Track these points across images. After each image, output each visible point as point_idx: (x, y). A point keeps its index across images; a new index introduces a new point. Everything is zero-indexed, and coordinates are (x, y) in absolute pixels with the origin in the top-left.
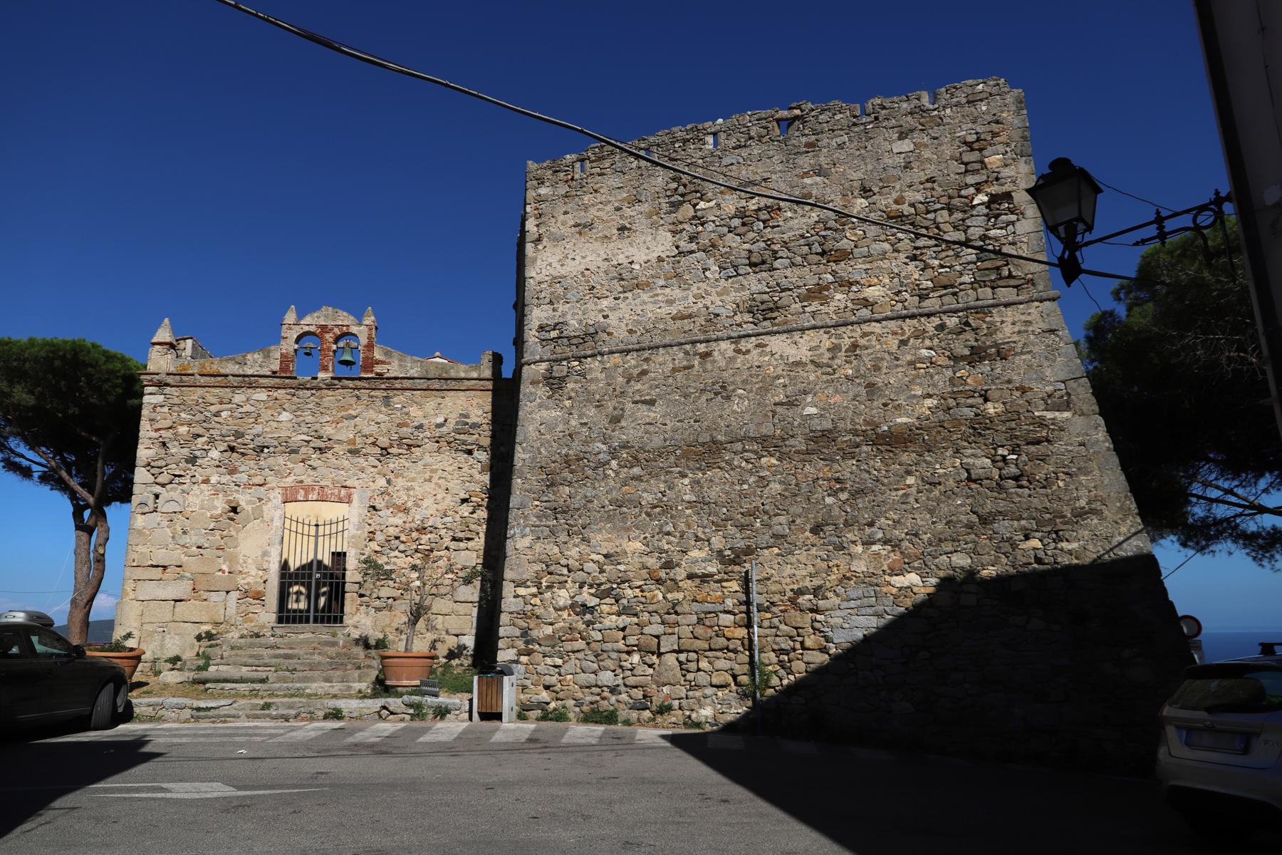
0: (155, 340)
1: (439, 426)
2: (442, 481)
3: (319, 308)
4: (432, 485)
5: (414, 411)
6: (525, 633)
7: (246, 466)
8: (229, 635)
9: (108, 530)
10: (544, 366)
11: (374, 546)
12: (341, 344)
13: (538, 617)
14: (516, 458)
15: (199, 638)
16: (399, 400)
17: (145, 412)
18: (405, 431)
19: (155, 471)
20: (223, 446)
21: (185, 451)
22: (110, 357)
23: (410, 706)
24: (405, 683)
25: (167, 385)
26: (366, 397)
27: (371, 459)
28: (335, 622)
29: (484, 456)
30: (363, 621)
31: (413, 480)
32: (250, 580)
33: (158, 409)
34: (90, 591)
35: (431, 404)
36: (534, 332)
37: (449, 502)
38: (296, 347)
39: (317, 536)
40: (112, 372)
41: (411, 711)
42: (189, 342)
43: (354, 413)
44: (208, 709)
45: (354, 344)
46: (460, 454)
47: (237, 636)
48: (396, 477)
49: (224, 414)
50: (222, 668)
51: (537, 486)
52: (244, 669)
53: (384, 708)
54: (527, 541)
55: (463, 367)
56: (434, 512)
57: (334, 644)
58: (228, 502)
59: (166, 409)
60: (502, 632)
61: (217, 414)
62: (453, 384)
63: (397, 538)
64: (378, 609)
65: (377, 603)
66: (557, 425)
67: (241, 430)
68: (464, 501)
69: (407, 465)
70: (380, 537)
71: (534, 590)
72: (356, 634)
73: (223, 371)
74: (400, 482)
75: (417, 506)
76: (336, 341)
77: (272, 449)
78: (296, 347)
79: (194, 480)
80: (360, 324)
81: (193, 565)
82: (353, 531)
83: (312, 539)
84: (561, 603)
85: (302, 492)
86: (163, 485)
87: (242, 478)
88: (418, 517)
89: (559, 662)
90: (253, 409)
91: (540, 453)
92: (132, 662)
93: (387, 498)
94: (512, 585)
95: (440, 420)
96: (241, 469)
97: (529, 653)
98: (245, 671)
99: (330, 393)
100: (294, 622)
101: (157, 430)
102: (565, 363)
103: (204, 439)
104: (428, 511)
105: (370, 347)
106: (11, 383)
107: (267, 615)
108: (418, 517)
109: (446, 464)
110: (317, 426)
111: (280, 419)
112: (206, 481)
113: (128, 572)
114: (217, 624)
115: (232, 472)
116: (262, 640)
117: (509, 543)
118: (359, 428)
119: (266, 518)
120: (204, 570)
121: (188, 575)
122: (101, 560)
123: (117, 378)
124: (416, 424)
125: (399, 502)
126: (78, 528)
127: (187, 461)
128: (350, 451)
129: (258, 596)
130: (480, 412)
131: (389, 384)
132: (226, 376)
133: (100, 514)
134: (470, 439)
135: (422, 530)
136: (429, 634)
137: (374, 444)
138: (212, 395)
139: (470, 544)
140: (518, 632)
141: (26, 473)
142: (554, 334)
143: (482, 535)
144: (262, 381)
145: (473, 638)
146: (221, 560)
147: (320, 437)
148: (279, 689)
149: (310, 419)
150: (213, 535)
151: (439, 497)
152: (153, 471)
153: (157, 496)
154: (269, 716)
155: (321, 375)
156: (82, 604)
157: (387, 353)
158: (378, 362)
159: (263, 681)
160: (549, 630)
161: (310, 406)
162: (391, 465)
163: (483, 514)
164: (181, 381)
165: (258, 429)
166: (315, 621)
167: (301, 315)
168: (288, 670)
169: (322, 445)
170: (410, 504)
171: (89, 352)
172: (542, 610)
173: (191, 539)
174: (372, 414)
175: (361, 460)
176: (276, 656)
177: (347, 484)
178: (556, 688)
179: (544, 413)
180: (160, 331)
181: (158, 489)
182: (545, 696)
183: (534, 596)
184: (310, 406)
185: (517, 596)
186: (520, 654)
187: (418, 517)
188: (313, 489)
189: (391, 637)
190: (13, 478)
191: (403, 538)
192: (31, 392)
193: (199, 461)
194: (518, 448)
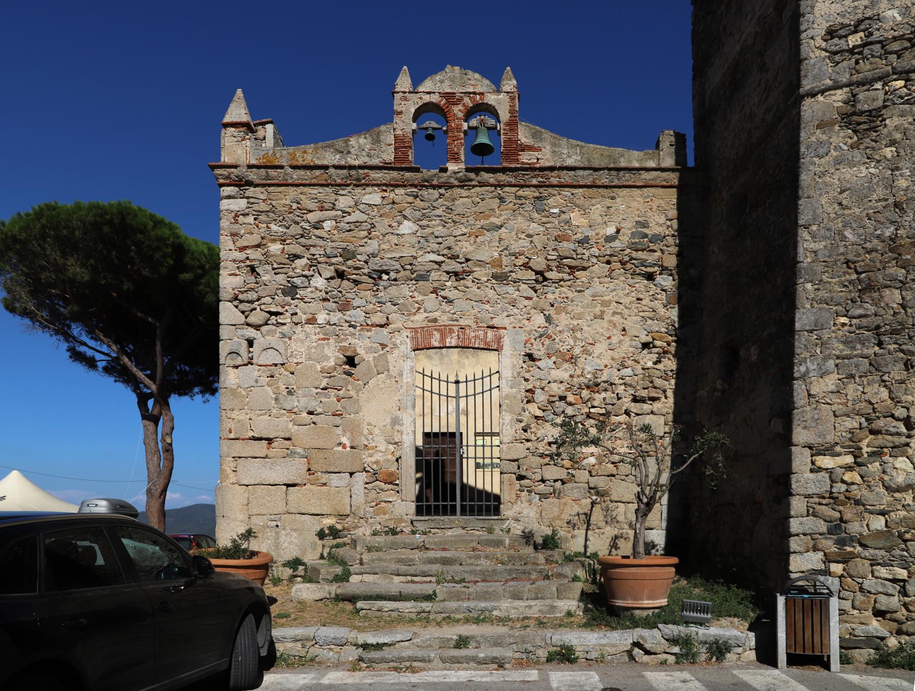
0: (227, 119)
1: (610, 239)
2: (617, 318)
3: (442, 69)
4: (605, 324)
5: (576, 217)
6: (837, 528)
7: (362, 298)
8: (359, 532)
9: (172, 420)
10: (840, 95)
11: (534, 409)
12: (474, 122)
13: (858, 502)
14: (801, 250)
15: (321, 535)
16: (555, 202)
17: (225, 223)
18: (566, 247)
19: (245, 307)
20: (329, 272)
21: (281, 278)
22: (158, 223)
23: (673, 641)
24: (647, 603)
25: (250, 184)
26: (510, 199)
27: (523, 287)
28: (488, 512)
29: (667, 282)
30: (525, 512)
31: (579, 316)
32: (378, 457)
33: (241, 219)
34: (162, 482)
35: (597, 209)
36: (819, 42)
37: (627, 347)
38: (414, 126)
39: (457, 397)
40: (161, 239)
41: (676, 650)
42: (270, 128)
43: (497, 221)
44: (379, 647)
45: (491, 122)
46: (638, 279)
47: (368, 532)
48: (558, 313)
49: (328, 225)
50: (368, 578)
51: (840, 293)
52: (397, 579)
53: (636, 644)
54: (831, 382)
55: (636, 154)
56: (607, 361)
57: (498, 543)
58: (342, 349)
59: (250, 219)
60: (795, 525)
61: (318, 225)
62: (627, 178)
63: (562, 398)
64: (543, 496)
65: (541, 487)
66: (871, 190)
67: (351, 247)
68: (645, 346)
69: (571, 295)
70: (540, 397)
71: (849, 459)
72: (517, 529)
73: (318, 162)
74: (563, 320)
75: (586, 352)
76: (467, 118)
77: (393, 275)
78: (414, 126)
79: (295, 319)
80: (498, 91)
81: (305, 437)
82: (506, 389)
83: (452, 403)
84: (900, 479)
85: (437, 335)
86: (257, 327)
87: (357, 315)
88: (589, 368)
89: (903, 574)
90: (363, 217)
91: (844, 238)
92: (259, 573)
93: (547, 342)
94: (807, 452)
95: (611, 230)
96: (355, 303)
97: (845, 559)
98: (396, 584)
99: (464, 193)
100: (437, 513)
101: (242, 249)
102: (878, 85)
103: (304, 261)
104: (599, 360)
105: (512, 125)
106: (64, 255)
107: (403, 505)
108: (588, 366)
109: (621, 293)
110: (451, 241)
111: (401, 231)
112: (312, 321)
113: (225, 446)
114: (342, 516)
115: (344, 307)
116: (399, 537)
117: (799, 388)
118: (505, 243)
119: (394, 371)
120: (319, 443)
121: (299, 450)
122: (169, 449)
123: (167, 246)
124: (579, 236)
125: (564, 348)
126: (144, 417)
127: (285, 293)
128: (495, 277)
129: (391, 480)
130: (662, 220)
131: (545, 178)
132: (326, 167)
133: (163, 401)
134: (651, 258)
135: (594, 387)
136: (608, 528)
137: (526, 266)
138: (308, 197)
139: (657, 406)
140: (823, 527)
141: (91, 363)
142: (854, 40)
143: (670, 393)
144: (375, 175)
145: (663, 533)
146: (339, 431)
147: (454, 257)
148: (457, 610)
149: (440, 230)
150: (326, 396)
151: (614, 340)
152: (243, 307)
153: (250, 343)
154: (475, 659)
155: (452, 167)
156: (157, 494)
157: (535, 135)
158: (525, 148)
159: (429, 598)
160: (879, 523)
161: (439, 212)
162: (550, 296)
163: (670, 364)
164: (268, 177)
165: (372, 246)
166: (463, 512)
167: (417, 81)
168: (453, 581)
169: (458, 268)
170: (577, 351)
171: (136, 216)
172: (865, 492)
173: (300, 402)
174: (520, 222)
175: (510, 289)
176: (432, 561)
177: (496, 322)
178: (899, 616)
179: (847, 173)
180: (232, 106)
181: (251, 333)
182: (875, 626)
183: (849, 468)
184: (439, 212)
185: (816, 470)
186: (828, 559)
187: (589, 368)
188: (451, 331)
189: (562, 533)
190: (79, 368)
191: (571, 398)
192: (83, 265)
193: (301, 292)
194: (803, 234)
